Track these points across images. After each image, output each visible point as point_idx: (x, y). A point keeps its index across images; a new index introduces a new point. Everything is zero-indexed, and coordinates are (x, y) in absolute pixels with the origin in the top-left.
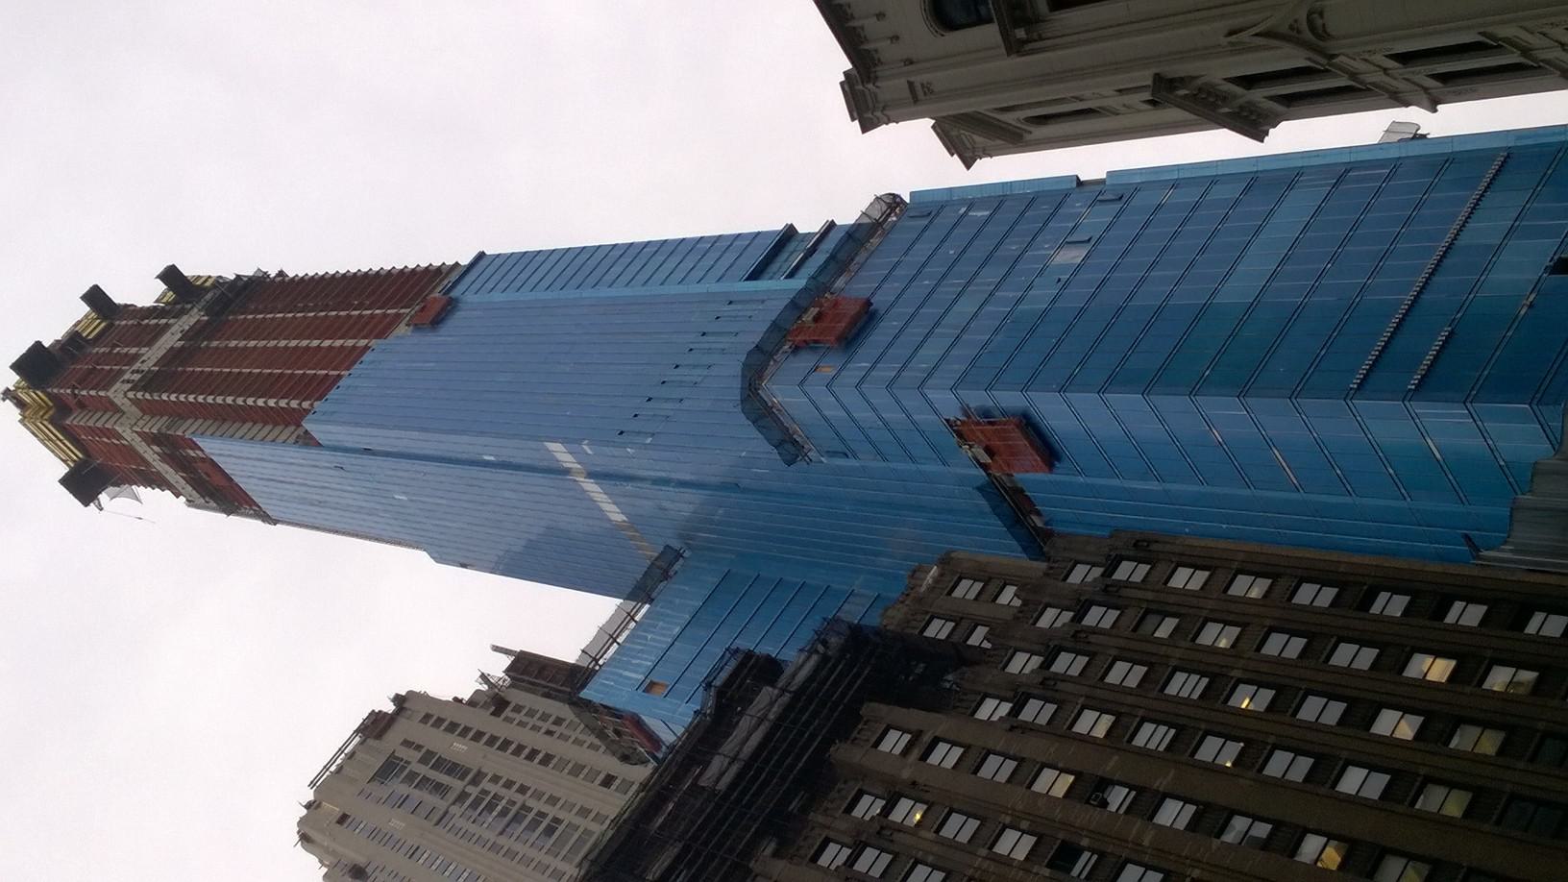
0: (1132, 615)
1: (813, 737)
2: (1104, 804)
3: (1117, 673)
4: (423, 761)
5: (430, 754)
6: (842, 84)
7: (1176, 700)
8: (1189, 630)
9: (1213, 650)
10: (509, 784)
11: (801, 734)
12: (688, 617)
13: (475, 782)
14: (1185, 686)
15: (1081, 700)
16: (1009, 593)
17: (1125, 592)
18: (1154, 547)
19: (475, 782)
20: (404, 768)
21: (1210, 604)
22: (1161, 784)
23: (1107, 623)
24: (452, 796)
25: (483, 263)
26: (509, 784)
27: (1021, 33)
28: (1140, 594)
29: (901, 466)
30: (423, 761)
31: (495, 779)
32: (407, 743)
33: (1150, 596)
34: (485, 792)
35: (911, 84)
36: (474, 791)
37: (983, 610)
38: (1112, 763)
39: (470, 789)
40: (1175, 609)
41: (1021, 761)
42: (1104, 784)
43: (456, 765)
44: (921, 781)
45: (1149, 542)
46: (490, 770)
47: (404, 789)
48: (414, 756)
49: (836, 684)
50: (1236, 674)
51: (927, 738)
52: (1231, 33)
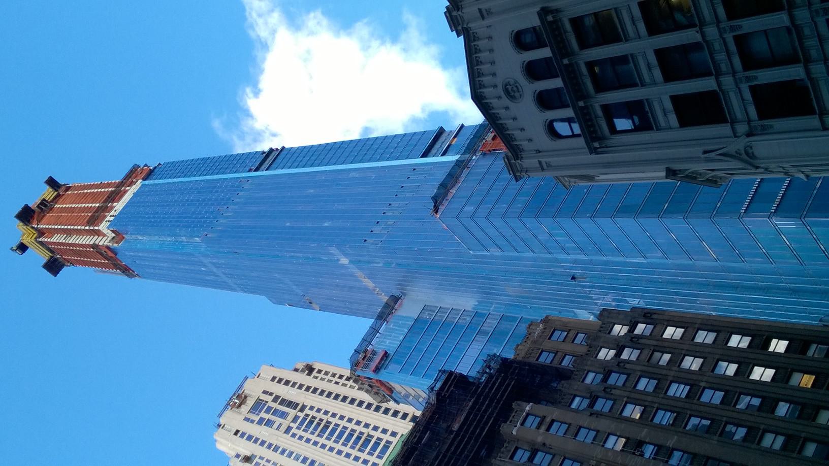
0: (647, 352)
1: (489, 418)
2: (642, 455)
3: (642, 384)
4: (275, 400)
5: (277, 397)
6: (445, 13)
7: (674, 398)
8: (677, 361)
9: (689, 371)
10: (319, 410)
11: (482, 417)
12: (406, 330)
13: (302, 410)
14: (678, 390)
15: (625, 399)
16: (581, 336)
17: (627, 366)
18: (655, 316)
19: (302, 410)
20: (265, 405)
21: (686, 347)
22: (670, 444)
23: (634, 358)
24: (290, 418)
25: (284, 152)
26: (319, 410)
27: (596, 145)
28: (648, 342)
29: (511, 254)
30: (275, 400)
31: (312, 408)
32: (265, 392)
33: (655, 343)
34: (307, 415)
35: (540, 162)
36: (302, 415)
37: (567, 347)
38: (644, 433)
39: (299, 414)
40: (668, 350)
41: (598, 431)
42: (640, 444)
43: (291, 402)
44: (547, 443)
45: (651, 314)
46: (309, 404)
47: (267, 416)
48: (271, 398)
49: (498, 389)
50: (703, 384)
51: (548, 420)
52: (705, 152)
